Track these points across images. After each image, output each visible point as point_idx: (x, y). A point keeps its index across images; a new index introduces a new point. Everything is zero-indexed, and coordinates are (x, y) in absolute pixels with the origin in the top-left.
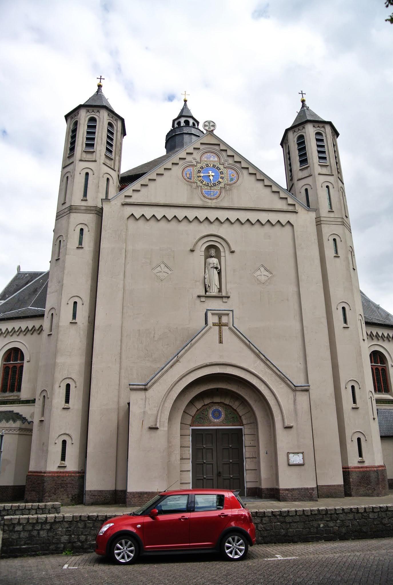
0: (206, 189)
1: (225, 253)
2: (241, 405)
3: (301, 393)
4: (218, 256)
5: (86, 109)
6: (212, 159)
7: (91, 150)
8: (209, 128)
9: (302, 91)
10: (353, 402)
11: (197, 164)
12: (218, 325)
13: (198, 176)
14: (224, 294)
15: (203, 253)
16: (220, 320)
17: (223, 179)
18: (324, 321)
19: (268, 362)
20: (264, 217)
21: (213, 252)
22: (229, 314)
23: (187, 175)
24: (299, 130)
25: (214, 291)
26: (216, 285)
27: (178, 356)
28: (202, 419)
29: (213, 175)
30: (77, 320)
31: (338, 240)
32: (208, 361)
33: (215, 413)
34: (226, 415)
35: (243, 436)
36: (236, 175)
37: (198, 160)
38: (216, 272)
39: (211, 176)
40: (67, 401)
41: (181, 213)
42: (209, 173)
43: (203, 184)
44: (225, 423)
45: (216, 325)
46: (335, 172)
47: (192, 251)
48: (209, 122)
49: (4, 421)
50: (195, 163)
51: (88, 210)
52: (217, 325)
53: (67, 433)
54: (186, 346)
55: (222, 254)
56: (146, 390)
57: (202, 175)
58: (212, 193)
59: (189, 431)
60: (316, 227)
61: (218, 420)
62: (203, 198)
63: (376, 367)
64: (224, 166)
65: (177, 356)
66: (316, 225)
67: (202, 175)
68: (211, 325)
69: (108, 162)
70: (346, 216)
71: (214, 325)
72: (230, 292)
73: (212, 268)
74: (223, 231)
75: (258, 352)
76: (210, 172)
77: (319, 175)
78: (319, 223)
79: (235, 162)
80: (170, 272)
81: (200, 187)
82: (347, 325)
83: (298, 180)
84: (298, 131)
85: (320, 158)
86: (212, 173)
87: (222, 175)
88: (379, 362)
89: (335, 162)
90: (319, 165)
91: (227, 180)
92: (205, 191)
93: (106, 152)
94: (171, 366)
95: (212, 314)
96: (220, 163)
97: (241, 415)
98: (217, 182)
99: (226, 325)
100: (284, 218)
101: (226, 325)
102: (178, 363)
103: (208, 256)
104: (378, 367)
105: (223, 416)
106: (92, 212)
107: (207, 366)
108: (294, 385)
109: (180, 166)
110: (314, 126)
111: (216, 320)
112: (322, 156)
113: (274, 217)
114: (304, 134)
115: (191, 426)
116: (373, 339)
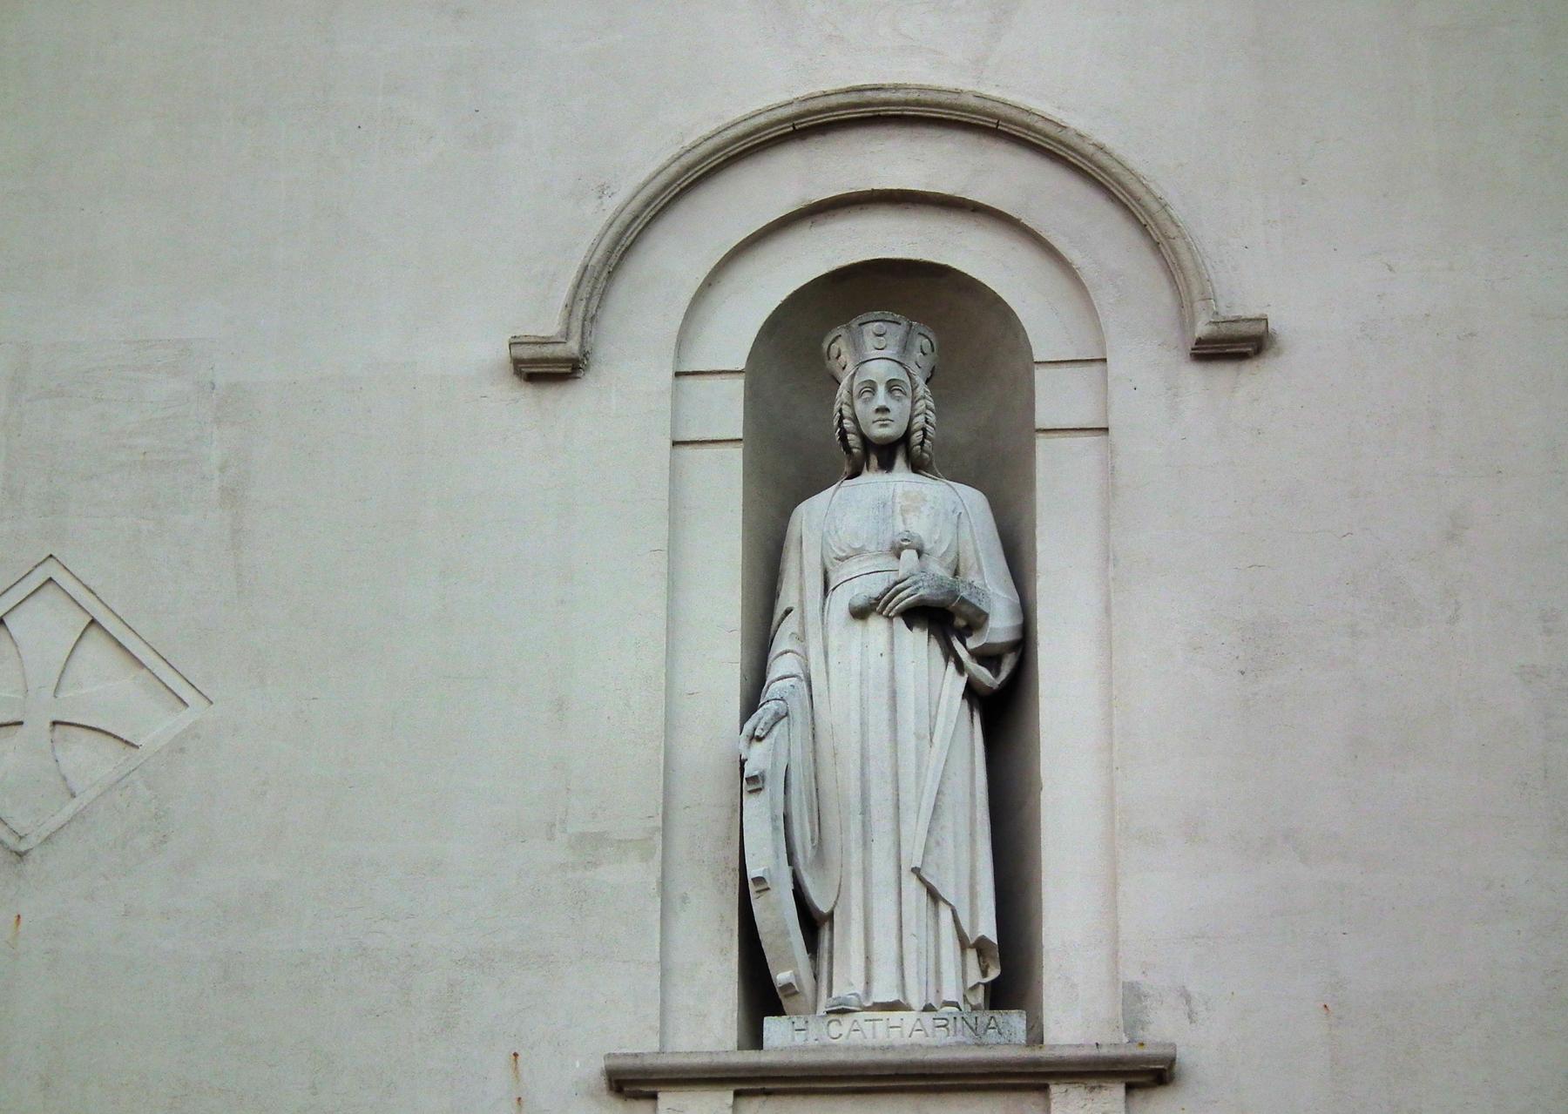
26: (934, 896)
73: (877, 625)
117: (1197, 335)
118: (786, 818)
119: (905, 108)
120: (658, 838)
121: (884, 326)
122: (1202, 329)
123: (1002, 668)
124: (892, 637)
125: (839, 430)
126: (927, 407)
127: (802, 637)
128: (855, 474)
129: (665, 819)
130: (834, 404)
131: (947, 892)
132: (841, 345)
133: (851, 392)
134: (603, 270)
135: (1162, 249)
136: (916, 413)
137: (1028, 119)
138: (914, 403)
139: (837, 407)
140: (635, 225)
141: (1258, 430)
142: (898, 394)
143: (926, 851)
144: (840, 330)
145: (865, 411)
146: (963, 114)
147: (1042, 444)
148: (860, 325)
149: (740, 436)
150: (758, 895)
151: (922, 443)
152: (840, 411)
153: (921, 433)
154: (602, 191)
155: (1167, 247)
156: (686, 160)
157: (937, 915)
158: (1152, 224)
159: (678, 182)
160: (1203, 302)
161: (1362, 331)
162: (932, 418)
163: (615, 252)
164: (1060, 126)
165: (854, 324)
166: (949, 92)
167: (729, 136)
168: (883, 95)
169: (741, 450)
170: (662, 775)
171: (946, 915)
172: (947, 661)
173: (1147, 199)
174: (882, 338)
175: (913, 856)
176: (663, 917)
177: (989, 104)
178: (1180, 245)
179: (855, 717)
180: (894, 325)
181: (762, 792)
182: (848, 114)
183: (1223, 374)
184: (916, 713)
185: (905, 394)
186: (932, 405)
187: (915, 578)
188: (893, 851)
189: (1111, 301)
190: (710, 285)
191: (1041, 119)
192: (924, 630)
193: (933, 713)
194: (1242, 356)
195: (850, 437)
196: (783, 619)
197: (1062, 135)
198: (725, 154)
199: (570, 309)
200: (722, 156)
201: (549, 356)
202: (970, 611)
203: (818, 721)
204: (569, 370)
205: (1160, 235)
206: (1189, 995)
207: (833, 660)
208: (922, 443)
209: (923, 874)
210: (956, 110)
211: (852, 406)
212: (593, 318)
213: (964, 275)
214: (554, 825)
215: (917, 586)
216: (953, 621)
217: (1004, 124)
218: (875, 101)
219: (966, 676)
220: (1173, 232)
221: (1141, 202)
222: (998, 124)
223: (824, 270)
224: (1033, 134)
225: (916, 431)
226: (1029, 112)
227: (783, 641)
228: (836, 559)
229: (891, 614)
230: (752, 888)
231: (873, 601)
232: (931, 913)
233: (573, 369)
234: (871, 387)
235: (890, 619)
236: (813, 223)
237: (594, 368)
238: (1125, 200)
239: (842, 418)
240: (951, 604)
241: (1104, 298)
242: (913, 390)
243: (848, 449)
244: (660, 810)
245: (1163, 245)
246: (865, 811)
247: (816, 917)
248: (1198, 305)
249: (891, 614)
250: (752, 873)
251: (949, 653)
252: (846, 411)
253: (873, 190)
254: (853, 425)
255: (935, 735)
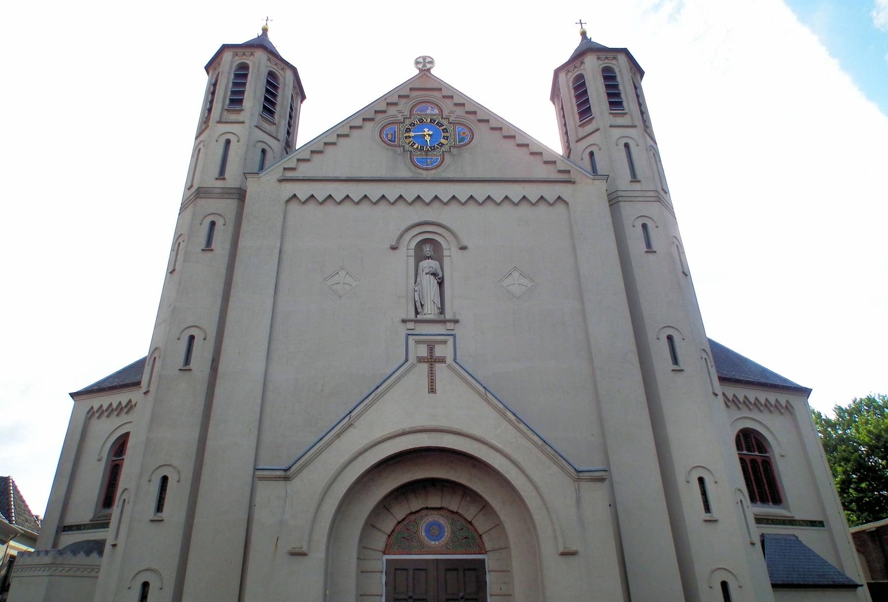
0: (419, 155)
1: (450, 251)
2: (481, 513)
3: (590, 484)
4: (437, 255)
5: (234, 52)
6: (430, 111)
7: (238, 108)
8: (424, 66)
9: (580, 20)
10: (705, 509)
11: (404, 120)
12: (428, 361)
13: (406, 137)
14: (448, 315)
15: (412, 253)
16: (431, 353)
17: (447, 139)
18: (634, 358)
19: (522, 426)
20: (515, 192)
21: (427, 249)
22: (447, 342)
23: (387, 136)
24: (575, 67)
25: (430, 311)
26: (434, 303)
27: (351, 416)
28: (407, 540)
29: (431, 133)
30: (193, 364)
31: (650, 225)
32: (407, 425)
33: (431, 529)
34: (453, 532)
35: (486, 574)
36: (468, 133)
37: (407, 113)
38: (434, 282)
39: (427, 136)
40: (160, 508)
41: (375, 191)
42: (425, 131)
43: (413, 149)
44: (451, 548)
45: (424, 362)
46: (639, 122)
47: (394, 248)
48: (424, 58)
49: (82, 553)
50: (401, 118)
51: (226, 193)
52: (425, 360)
53: (153, 567)
54: (367, 397)
55: (446, 253)
56: (286, 479)
57: (412, 134)
58: (429, 160)
59: (380, 562)
60: (610, 209)
61: (437, 543)
62: (413, 168)
63: (752, 457)
64: (449, 120)
65: (349, 416)
66: (607, 201)
67: (412, 134)
68: (415, 362)
69: (266, 126)
70: (663, 190)
71: (420, 362)
72: (460, 314)
73: (428, 275)
74: (444, 215)
75: (501, 406)
76: (426, 130)
77: (611, 128)
78: (614, 201)
79: (467, 113)
80: (354, 284)
81: (409, 152)
82: (679, 366)
83: (577, 142)
84: (573, 70)
85: (611, 103)
86: (428, 131)
87: (446, 134)
88: (756, 450)
89: (639, 111)
90: (610, 113)
91: (454, 141)
92: (418, 158)
93: (263, 111)
94: (338, 436)
95: (415, 342)
96: (442, 116)
97: (481, 533)
98: (438, 145)
99: (442, 360)
100: (550, 192)
101: (442, 361)
102: (351, 429)
103: (420, 257)
104: (755, 457)
105: (447, 534)
106: (232, 197)
107: (404, 433)
108: (575, 469)
109: (378, 123)
110: (598, 58)
111: (423, 351)
112: (615, 101)
113: (533, 192)
114: (584, 73)
115: (384, 553)
116: (739, 408)
122: (460, 246)
147: (445, 258)
175: (432, 299)
183: (462, 251)
226: (789, 394)
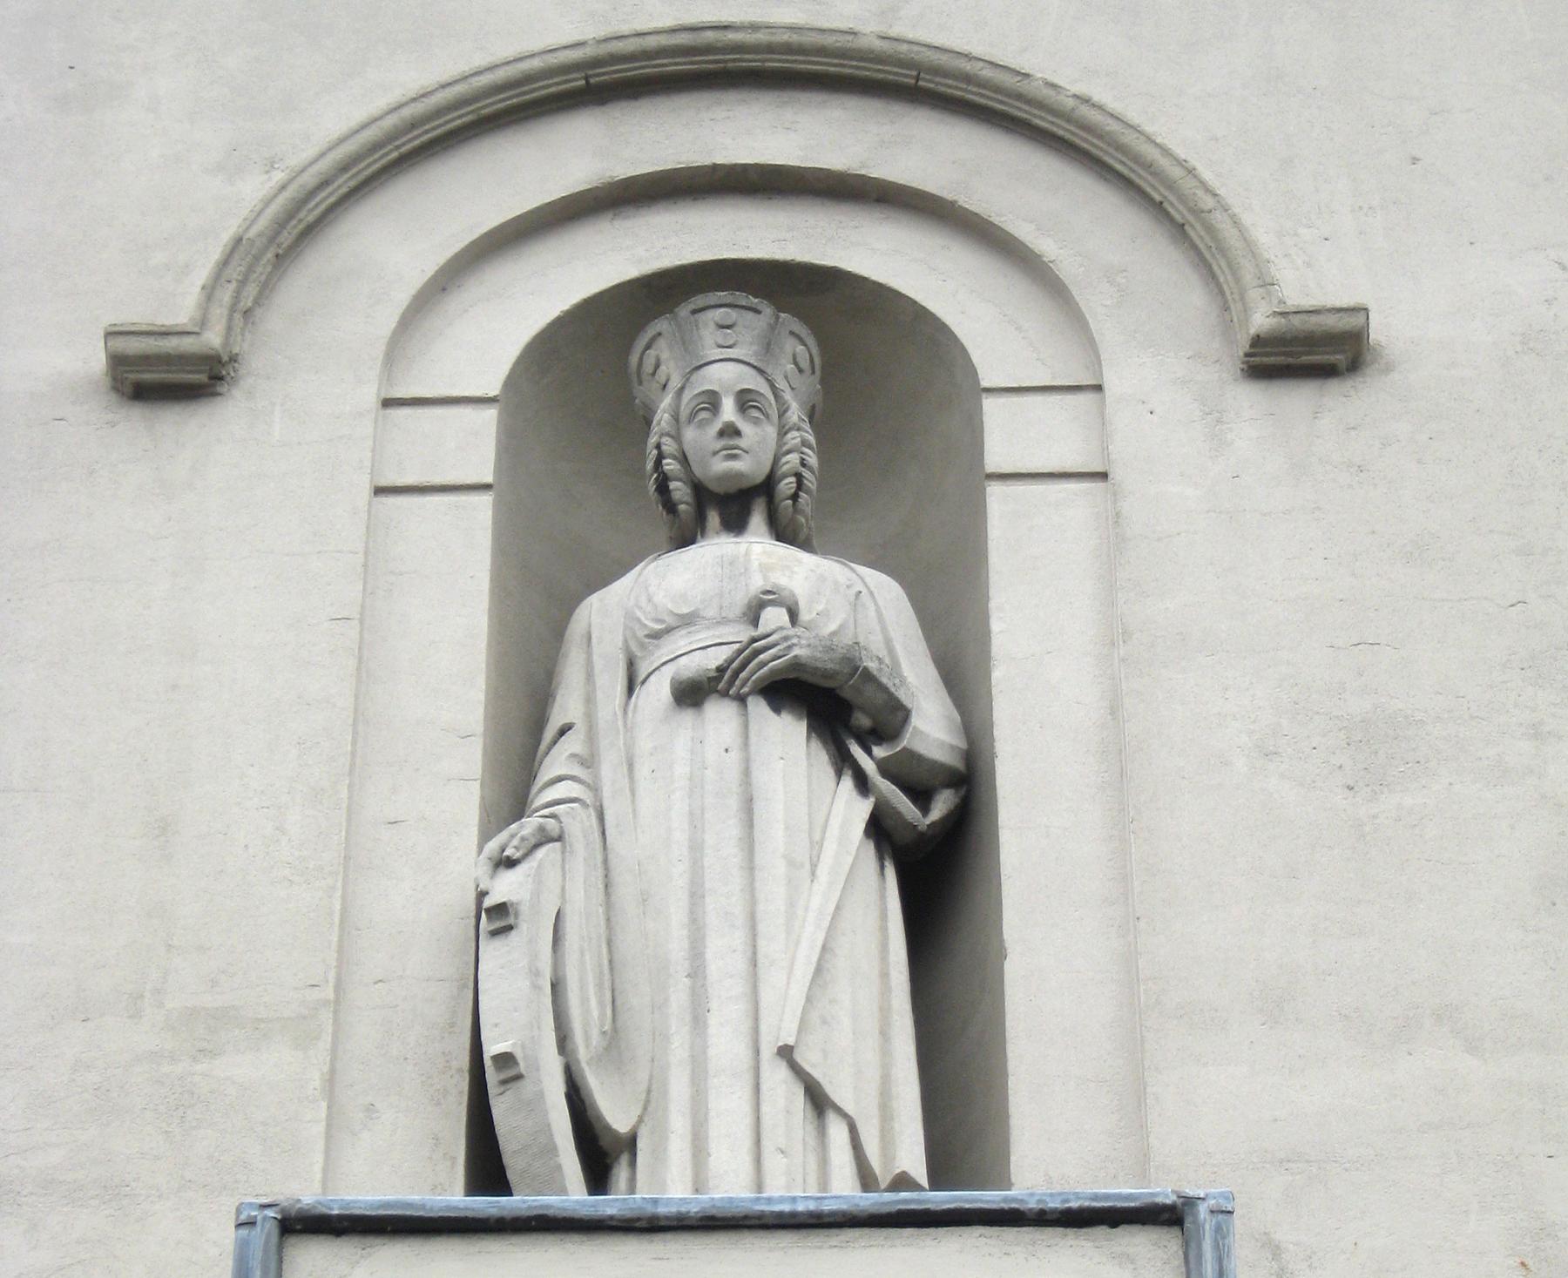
26: (818, 1101)
73: (719, 715)
117: (1253, 331)
118: (557, 987)
119: (769, 56)
120: (326, 1016)
121: (733, 315)
122: (1261, 320)
123: (932, 806)
124: (746, 726)
125: (655, 476)
126: (804, 443)
127: (588, 761)
128: (684, 539)
129: (339, 988)
130: (647, 435)
131: (839, 1091)
132: (663, 350)
133: (676, 418)
134: (266, 248)
135: (1192, 234)
136: (785, 448)
137: (967, 67)
138: (783, 432)
139: (653, 440)
140: (323, 194)
141: (1359, 467)
142: (755, 413)
143: (800, 1030)
144: (662, 325)
145: (700, 438)
146: (862, 64)
147: (998, 497)
148: (694, 312)
149: (489, 479)
150: (502, 1089)
151: (795, 497)
152: (658, 446)
153: (793, 479)
154: (271, 165)
155: (1198, 226)
156: (407, 112)
157: (822, 1131)
158: (1172, 198)
159: (397, 143)
160: (1261, 290)
161: (1523, 343)
162: (810, 480)
163: (289, 227)
164: (1018, 73)
165: (684, 311)
166: (841, 32)
167: (480, 84)
168: (732, 36)
169: (491, 498)
170: (336, 928)
171: (838, 1132)
172: (839, 774)
173: (1163, 162)
174: (729, 331)
175: (781, 1027)
176: (328, 1137)
177: (904, 48)
178: (1219, 219)
179: (680, 836)
180: (750, 315)
181: (513, 933)
182: (676, 64)
183: (1296, 398)
184: (787, 828)
185: (767, 416)
186: (811, 439)
187: (784, 633)
188: (746, 1026)
189: (1108, 303)
190: (444, 289)
191: (986, 65)
192: (800, 718)
193: (817, 837)
194: (1326, 372)
195: (673, 485)
196: (555, 742)
197: (1024, 87)
198: (472, 112)
199: (210, 291)
200: (468, 113)
201: (171, 352)
202: (880, 699)
203: (614, 861)
204: (202, 378)
205: (1185, 212)
206: (1278, 1247)
207: (643, 771)
208: (795, 497)
209: (798, 1057)
210: (852, 59)
211: (677, 438)
212: (247, 313)
213: (865, 279)
214: (142, 996)
215: (789, 643)
216: (850, 716)
217: (928, 77)
218: (719, 45)
219: (872, 799)
220: (1209, 202)
221: (1152, 169)
222: (917, 78)
223: (632, 272)
224: (975, 89)
225: (785, 476)
226: (968, 57)
227: (556, 763)
228: (648, 636)
229: (746, 690)
230: (492, 1076)
231: (713, 674)
232: (812, 1142)
233: (212, 378)
234: (711, 401)
235: (742, 700)
236: (615, 215)
237: (247, 383)
238: (1125, 171)
239: (660, 457)
240: (846, 682)
241: (1094, 301)
242: (782, 414)
243: (670, 506)
244: (332, 975)
245: (1192, 226)
246: (697, 972)
247: (605, 1142)
248: (1254, 294)
249: (746, 690)
250: (491, 1049)
251: (843, 762)
252: (669, 446)
253: (715, 164)
254: (679, 467)
255: (820, 866)
